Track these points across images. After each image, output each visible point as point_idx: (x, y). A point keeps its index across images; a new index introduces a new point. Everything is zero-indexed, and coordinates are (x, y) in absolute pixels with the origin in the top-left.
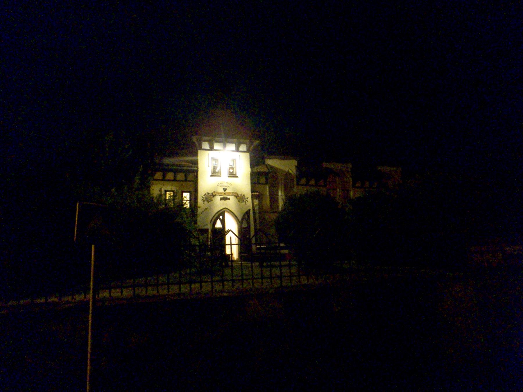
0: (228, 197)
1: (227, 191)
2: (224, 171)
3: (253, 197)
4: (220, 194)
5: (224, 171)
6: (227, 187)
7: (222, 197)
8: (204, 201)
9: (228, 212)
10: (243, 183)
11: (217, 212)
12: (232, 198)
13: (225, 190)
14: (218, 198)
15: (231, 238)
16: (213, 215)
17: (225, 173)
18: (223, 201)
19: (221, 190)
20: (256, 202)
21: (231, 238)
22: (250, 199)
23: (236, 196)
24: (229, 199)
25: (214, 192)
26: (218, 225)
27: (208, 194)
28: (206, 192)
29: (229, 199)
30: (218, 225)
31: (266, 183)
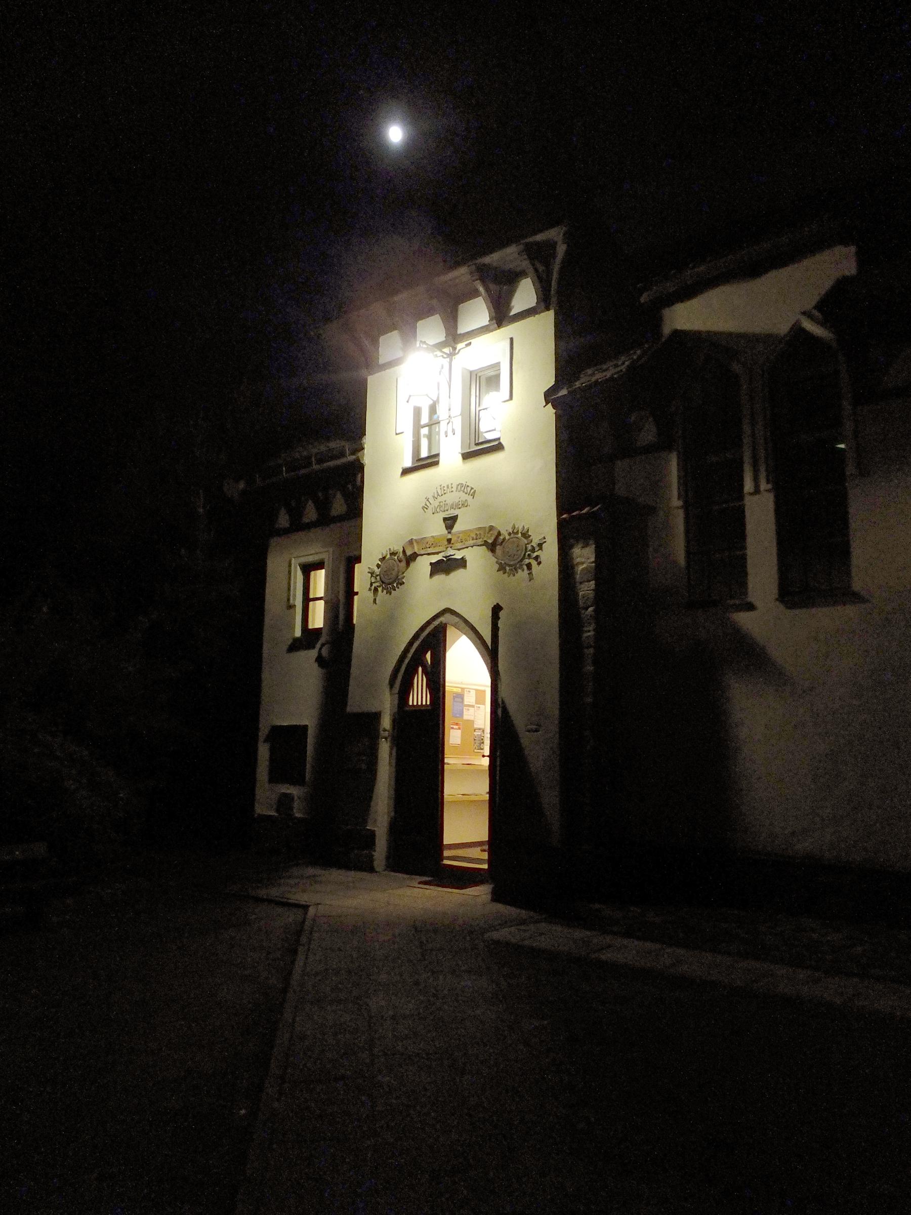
0: (458, 556)
1: (457, 528)
2: (395, 134)
3: (567, 535)
4: (428, 545)
5: (395, 134)
6: (457, 506)
7: (435, 558)
8: (376, 590)
9: (455, 626)
10: (523, 479)
11: (423, 629)
12: (477, 559)
13: (450, 522)
14: (423, 565)
15: (438, 384)
16: (402, 647)
17: (450, 450)
18: (440, 578)
19: (437, 529)
20: (584, 556)
21: (438, 384)
22: (550, 553)
23: (493, 544)
24: (462, 563)
25: (411, 542)
26: (420, 696)
27: (393, 554)
28: (385, 551)
29: (462, 563)
30: (420, 696)
31: (664, 444)
